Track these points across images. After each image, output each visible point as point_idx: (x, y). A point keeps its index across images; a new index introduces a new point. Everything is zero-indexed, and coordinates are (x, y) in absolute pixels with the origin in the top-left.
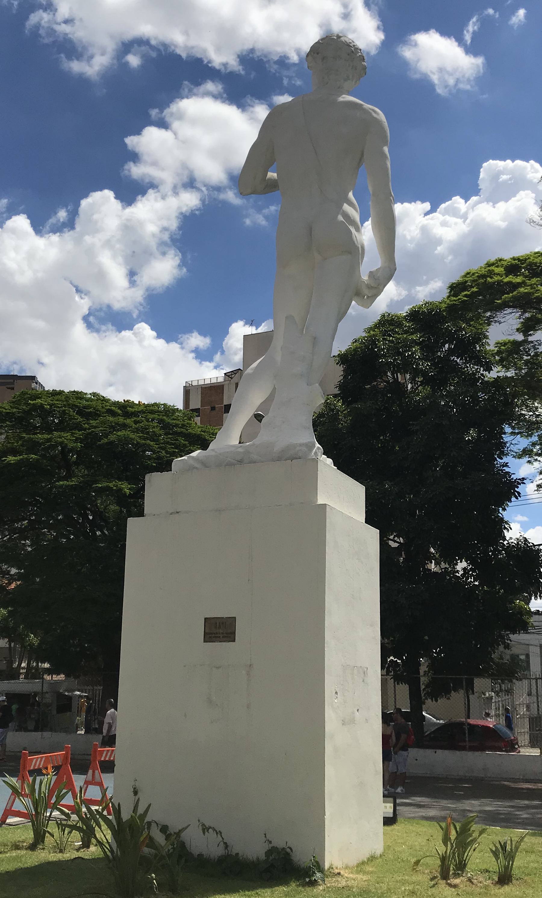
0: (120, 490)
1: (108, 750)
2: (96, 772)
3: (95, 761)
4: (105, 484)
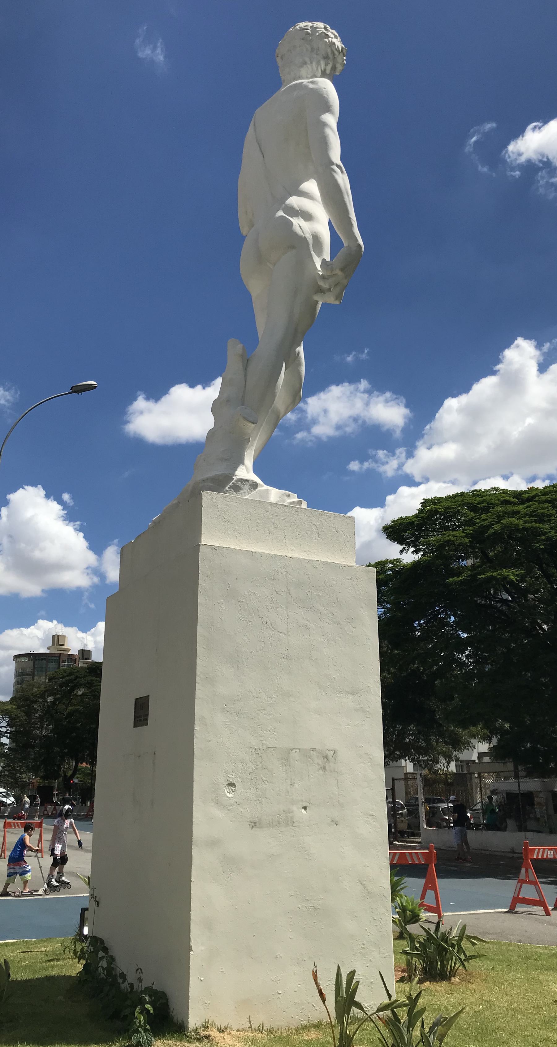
0: (505, 578)
1: (539, 849)
2: (529, 870)
3: (527, 859)
4: (488, 574)
